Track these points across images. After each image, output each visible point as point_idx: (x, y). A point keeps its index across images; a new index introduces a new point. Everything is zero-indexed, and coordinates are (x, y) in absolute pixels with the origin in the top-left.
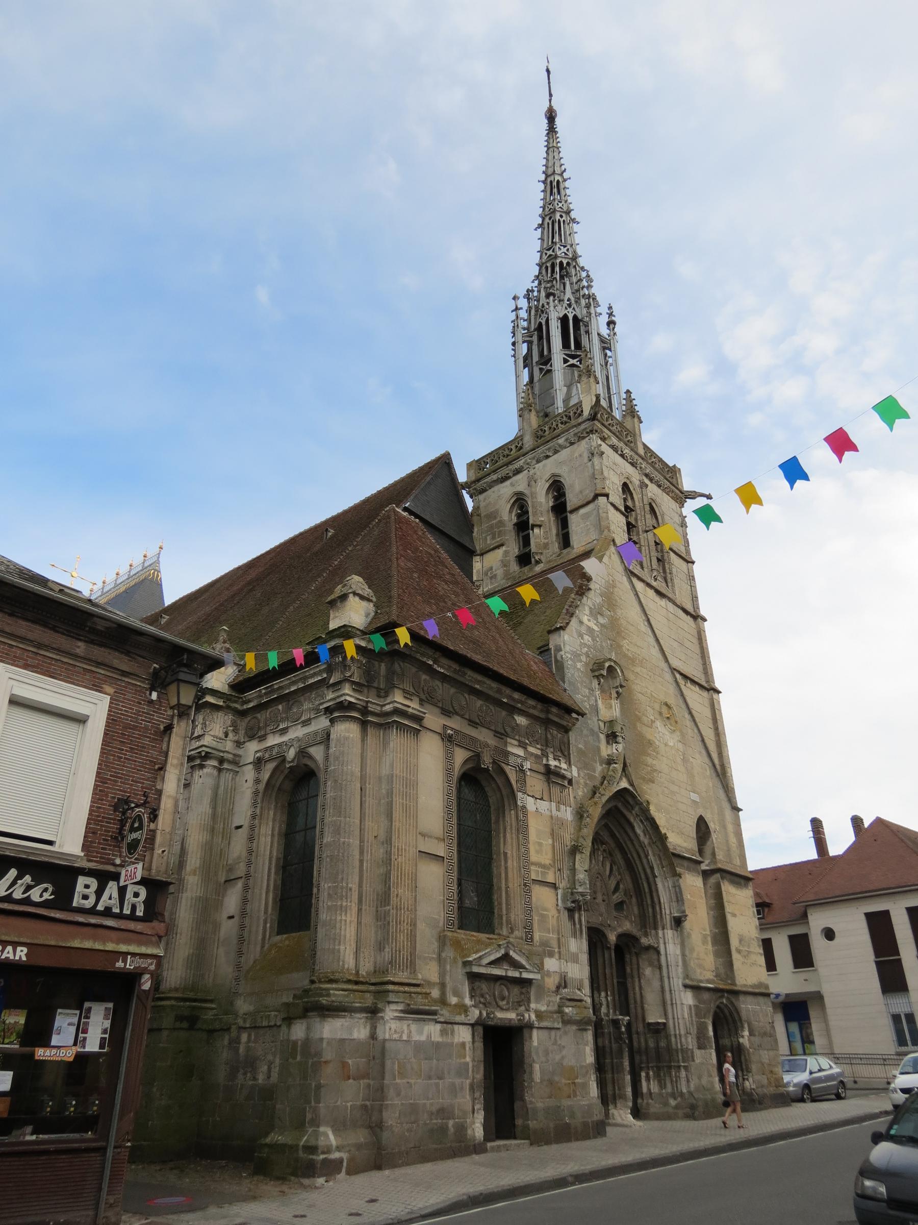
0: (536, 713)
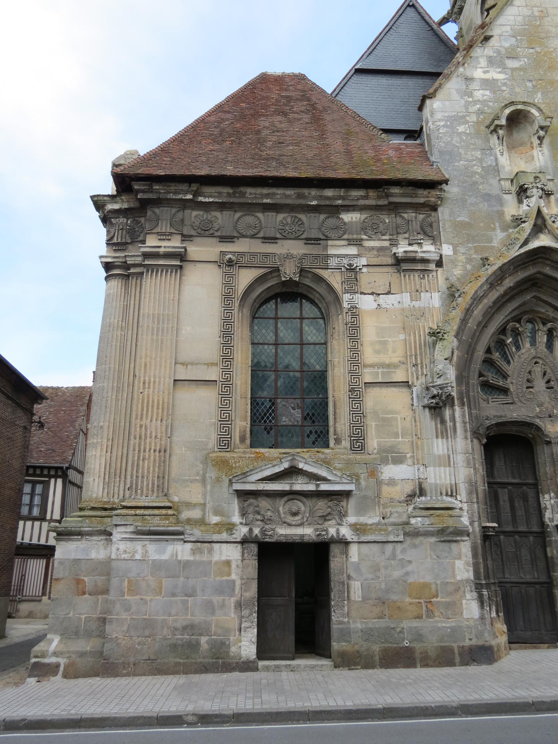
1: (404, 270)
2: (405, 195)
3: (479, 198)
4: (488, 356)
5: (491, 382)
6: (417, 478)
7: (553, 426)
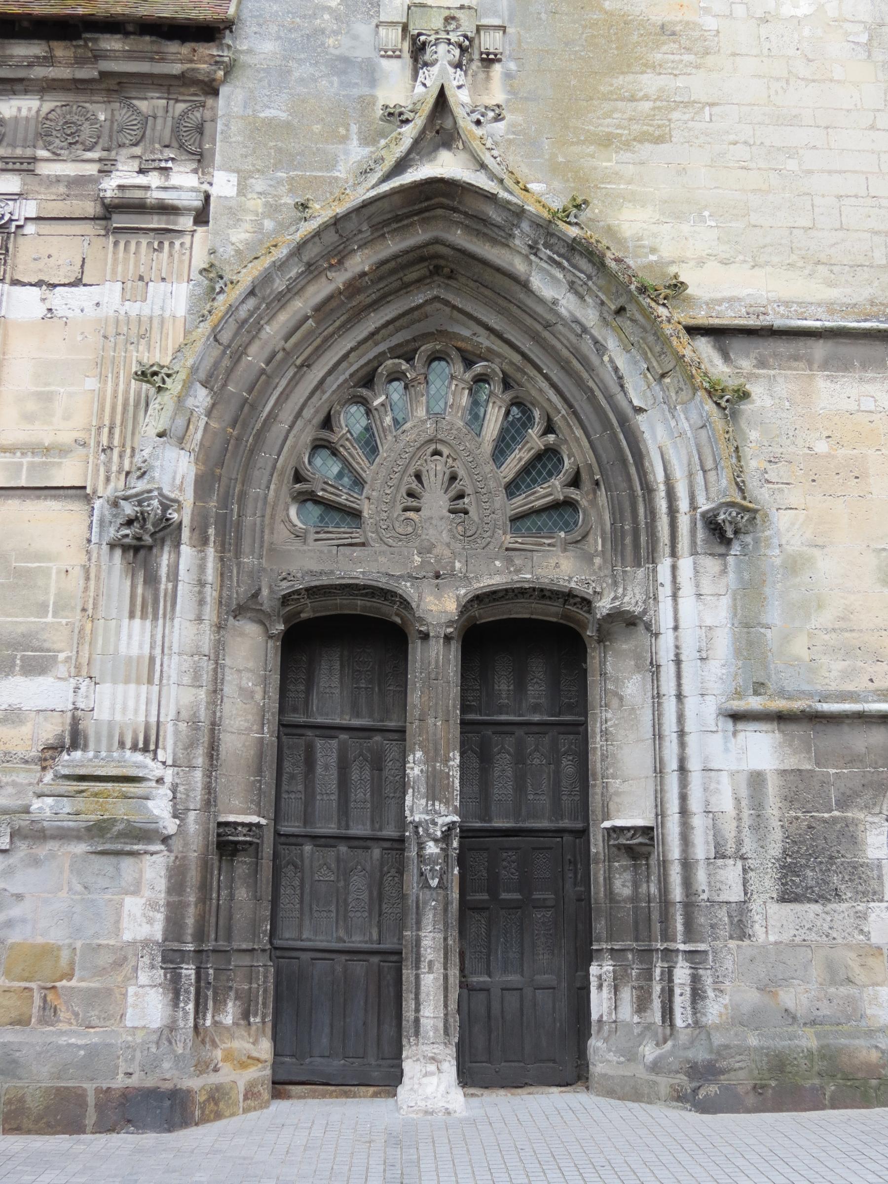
0: (62, 72)
1: (117, 231)
2: (136, 55)
3: (323, 68)
4: (325, 434)
5: (320, 494)
6: (71, 707)
7: (439, 597)
